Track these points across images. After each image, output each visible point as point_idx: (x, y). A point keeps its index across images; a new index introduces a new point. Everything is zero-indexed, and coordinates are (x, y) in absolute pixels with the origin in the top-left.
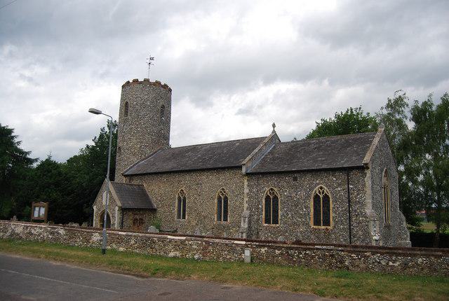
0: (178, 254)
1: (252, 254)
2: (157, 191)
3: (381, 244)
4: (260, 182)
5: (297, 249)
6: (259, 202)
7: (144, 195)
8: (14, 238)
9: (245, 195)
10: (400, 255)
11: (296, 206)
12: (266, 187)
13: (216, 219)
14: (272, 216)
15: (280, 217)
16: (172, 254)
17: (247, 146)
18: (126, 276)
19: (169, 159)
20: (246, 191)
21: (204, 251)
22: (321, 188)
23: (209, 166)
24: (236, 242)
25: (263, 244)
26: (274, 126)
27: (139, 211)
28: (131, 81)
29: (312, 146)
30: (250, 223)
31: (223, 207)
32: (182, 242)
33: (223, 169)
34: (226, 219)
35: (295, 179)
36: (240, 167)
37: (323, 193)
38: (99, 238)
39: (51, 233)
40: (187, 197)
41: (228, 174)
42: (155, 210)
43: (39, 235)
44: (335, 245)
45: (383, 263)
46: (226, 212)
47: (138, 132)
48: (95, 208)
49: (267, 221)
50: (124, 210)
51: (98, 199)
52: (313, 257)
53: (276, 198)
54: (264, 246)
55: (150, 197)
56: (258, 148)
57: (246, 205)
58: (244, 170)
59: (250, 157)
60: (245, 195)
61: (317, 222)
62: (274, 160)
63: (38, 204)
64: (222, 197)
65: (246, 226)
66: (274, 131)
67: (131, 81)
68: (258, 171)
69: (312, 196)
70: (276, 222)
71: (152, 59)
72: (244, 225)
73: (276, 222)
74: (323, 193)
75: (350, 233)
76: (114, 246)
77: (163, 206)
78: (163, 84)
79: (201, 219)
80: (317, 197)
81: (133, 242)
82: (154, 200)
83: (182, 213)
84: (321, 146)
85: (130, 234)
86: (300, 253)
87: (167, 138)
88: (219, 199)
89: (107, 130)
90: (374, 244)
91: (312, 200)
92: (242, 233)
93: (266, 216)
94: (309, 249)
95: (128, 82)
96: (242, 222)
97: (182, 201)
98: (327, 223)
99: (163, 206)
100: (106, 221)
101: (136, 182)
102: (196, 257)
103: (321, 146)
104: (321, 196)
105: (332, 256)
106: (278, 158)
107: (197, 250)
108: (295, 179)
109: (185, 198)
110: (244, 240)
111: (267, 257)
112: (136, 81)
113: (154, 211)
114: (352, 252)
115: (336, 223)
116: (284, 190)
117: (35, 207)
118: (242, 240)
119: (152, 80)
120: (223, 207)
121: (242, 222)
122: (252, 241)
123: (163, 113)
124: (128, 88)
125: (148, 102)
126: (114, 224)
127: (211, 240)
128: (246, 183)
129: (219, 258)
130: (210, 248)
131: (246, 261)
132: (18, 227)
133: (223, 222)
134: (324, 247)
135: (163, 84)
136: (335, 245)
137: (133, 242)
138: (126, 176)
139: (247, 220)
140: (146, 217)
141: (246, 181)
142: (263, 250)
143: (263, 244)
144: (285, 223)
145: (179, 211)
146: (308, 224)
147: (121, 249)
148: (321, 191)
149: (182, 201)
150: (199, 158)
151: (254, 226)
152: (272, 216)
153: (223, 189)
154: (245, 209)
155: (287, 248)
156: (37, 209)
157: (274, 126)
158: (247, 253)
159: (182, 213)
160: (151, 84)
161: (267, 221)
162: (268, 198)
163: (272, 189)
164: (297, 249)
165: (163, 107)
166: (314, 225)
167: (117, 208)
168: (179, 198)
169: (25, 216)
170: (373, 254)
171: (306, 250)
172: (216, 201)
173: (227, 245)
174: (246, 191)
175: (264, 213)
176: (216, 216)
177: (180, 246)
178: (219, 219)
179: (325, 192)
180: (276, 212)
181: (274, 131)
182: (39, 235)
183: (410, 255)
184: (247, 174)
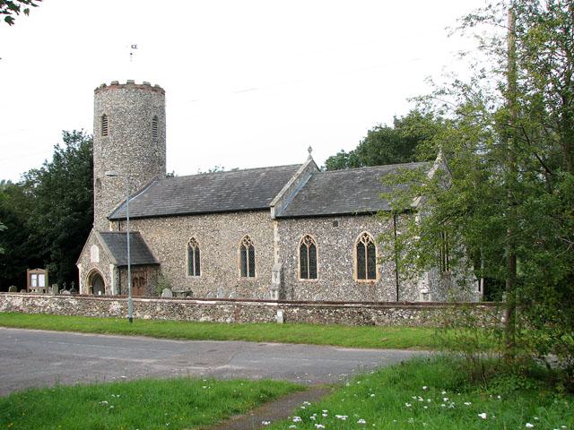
0: (209, 318)
1: (284, 314)
2: (162, 240)
3: (430, 301)
4: (294, 228)
5: (327, 308)
6: (293, 253)
7: (139, 244)
8: (12, 311)
9: (276, 244)
10: (420, 309)
11: (337, 256)
12: (301, 231)
13: (240, 275)
14: (309, 270)
15: (318, 271)
16: (203, 319)
17: (276, 177)
18: (27, 330)
19: (171, 196)
20: (277, 239)
21: (237, 315)
22: (366, 235)
23: (227, 208)
24: (268, 304)
25: (296, 304)
26: (310, 150)
27: (141, 269)
28: (108, 84)
29: (358, 179)
30: (282, 278)
31: (249, 261)
32: (213, 307)
33: (247, 211)
34: (252, 274)
35: (335, 224)
36: (268, 210)
37: (368, 240)
38: (119, 306)
39: (60, 304)
40: (200, 247)
41: (252, 217)
42: (158, 265)
43: (45, 307)
44: (363, 303)
45: (405, 317)
46: (252, 266)
47: (124, 157)
48: (79, 266)
49: (304, 275)
50: (121, 268)
51: (84, 255)
52: (342, 315)
53: (313, 247)
54: (296, 307)
55: (150, 248)
56: (290, 183)
57: (277, 257)
58: (273, 213)
59: (280, 195)
60: (276, 244)
61: (361, 275)
62: (310, 199)
63: (34, 271)
64: (247, 247)
65: (278, 282)
66: (310, 157)
67: (108, 84)
68: (291, 214)
69: (356, 245)
70: (314, 275)
71: (134, 47)
72: (276, 281)
73: (314, 275)
74: (368, 240)
75: (398, 286)
76: (138, 315)
77: (168, 260)
78: (153, 85)
79: (221, 275)
80: (360, 245)
81: (158, 309)
82: (155, 252)
83: (195, 267)
84: (367, 180)
85: (155, 300)
86: (330, 312)
87: (162, 162)
88: (243, 249)
89: (64, 146)
90: (421, 299)
91: (355, 248)
92: (274, 291)
93: (302, 269)
94: (339, 308)
95: (105, 86)
96: (273, 276)
97: (195, 255)
98: (372, 275)
99: (168, 260)
100: (96, 280)
101: (128, 227)
102: (228, 320)
103: (367, 180)
104: (366, 245)
105: (360, 313)
106: (315, 196)
107: (229, 314)
108: (335, 224)
109: (197, 249)
110: (277, 302)
111: (300, 317)
112: (116, 85)
113: (157, 266)
114: (380, 308)
115: (383, 275)
116: (323, 236)
117: (31, 275)
118: (274, 302)
119: (139, 82)
120: (249, 261)
121: (273, 276)
122: (284, 302)
123: (155, 127)
124: (104, 94)
125: (139, 111)
126: (109, 287)
127: (243, 303)
128: (276, 229)
129: (251, 320)
130: (242, 311)
131: (279, 321)
132: (16, 299)
133: (249, 279)
134: (353, 305)
135: (153, 85)
136: (363, 303)
137: (158, 309)
138: (112, 220)
139: (279, 274)
140: (149, 275)
141: (276, 226)
142: (295, 311)
143: (296, 304)
144: (324, 277)
145: (191, 265)
146: (351, 278)
147: (146, 317)
148: (366, 239)
149: (195, 255)
150: (213, 194)
151: (288, 282)
152: (309, 270)
153: (247, 237)
154: (276, 261)
155: (318, 308)
156: (34, 277)
157: (310, 150)
158: (280, 314)
159: (195, 267)
160: (137, 87)
161: (304, 275)
162: (303, 247)
163: (308, 237)
164: (327, 308)
165: (155, 118)
166: (358, 278)
167: (112, 267)
168: (190, 249)
169: (22, 285)
170: (397, 310)
171: (336, 308)
172: (239, 252)
173: (259, 307)
174: (277, 239)
175: (299, 265)
176: (239, 270)
177: (211, 310)
178: (244, 274)
179: (370, 239)
180: (313, 263)
181: (310, 157)
182: (45, 307)
183: (429, 309)
184: (277, 218)
